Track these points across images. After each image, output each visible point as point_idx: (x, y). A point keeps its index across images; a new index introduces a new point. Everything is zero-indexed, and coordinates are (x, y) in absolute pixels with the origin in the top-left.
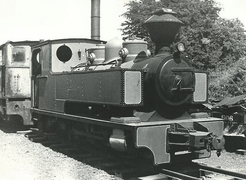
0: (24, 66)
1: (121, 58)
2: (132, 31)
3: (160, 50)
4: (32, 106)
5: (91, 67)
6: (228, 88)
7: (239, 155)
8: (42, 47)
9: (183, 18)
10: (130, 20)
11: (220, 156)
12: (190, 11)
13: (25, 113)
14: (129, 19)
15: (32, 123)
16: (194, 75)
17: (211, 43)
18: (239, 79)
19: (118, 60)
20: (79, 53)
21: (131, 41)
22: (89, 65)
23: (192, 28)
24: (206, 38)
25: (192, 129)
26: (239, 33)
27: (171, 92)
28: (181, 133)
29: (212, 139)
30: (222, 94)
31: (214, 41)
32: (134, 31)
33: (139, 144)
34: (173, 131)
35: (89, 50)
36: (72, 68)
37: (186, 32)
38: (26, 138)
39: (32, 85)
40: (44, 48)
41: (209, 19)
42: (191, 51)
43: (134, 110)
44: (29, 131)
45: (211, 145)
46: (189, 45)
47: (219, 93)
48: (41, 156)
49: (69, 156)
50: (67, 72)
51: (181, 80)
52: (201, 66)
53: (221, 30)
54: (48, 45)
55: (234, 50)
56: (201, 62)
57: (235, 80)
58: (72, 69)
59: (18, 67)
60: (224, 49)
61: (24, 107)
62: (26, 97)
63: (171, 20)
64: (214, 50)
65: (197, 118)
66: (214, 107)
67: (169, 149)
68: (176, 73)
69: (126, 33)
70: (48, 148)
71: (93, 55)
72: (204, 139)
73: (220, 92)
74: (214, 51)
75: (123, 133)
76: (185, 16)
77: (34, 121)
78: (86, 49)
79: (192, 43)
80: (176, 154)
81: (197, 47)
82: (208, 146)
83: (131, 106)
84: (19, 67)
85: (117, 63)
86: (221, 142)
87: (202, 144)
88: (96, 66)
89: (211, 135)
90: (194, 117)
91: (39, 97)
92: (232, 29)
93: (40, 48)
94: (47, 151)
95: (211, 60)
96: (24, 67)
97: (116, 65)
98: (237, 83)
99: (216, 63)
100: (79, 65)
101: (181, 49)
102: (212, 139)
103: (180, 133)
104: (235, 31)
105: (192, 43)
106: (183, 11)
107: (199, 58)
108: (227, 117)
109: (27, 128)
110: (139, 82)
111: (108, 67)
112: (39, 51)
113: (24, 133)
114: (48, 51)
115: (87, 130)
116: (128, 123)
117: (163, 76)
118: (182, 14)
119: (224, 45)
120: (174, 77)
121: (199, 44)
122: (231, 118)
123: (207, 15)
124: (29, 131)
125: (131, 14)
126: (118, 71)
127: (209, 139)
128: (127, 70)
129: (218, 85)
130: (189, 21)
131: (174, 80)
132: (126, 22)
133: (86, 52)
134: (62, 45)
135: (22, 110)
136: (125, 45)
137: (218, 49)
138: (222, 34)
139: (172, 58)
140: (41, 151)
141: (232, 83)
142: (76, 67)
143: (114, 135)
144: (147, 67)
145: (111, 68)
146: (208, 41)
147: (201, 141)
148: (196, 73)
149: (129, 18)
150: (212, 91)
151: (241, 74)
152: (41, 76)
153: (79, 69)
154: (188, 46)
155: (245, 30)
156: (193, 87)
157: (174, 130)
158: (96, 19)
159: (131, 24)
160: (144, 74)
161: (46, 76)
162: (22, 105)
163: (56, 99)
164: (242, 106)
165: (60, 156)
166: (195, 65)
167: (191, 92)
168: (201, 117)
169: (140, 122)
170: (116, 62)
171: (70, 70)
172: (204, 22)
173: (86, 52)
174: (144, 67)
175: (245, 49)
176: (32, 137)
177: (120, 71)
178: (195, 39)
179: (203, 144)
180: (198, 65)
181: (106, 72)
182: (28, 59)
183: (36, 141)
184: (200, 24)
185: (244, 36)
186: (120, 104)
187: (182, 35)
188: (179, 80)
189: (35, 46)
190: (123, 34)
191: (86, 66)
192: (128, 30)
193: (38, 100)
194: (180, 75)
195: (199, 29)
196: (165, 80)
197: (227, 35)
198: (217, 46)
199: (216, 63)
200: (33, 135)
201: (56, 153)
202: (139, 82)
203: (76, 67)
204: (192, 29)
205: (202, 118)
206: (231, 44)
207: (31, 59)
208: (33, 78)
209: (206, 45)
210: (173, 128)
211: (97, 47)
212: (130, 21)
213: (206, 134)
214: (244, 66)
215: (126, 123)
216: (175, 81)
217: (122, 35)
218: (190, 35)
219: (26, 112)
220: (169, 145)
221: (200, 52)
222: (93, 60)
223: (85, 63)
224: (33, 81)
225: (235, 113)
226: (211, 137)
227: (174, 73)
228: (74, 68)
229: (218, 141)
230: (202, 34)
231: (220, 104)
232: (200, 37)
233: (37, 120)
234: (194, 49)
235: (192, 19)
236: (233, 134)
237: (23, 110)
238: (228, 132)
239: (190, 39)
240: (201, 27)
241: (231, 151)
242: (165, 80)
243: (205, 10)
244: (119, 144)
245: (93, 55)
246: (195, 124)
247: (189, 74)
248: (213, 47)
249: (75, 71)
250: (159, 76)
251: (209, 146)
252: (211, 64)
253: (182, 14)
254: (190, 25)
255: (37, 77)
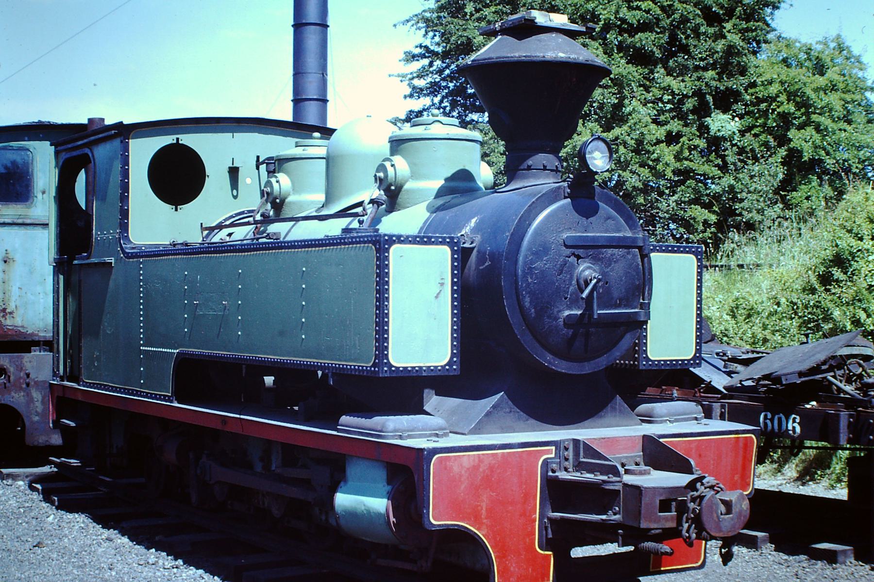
0: (28, 218)
1: (382, 192)
2: (444, 84)
3: (525, 166)
4: (55, 374)
5: (273, 228)
6: (798, 308)
7: (820, 564)
8: (132, 142)
9: (637, 36)
10: (437, 39)
11: (730, 564)
12: (663, 8)
13: (30, 400)
14: (433, 38)
15: (56, 439)
16: (646, 259)
17: (742, 133)
18: (837, 273)
19: (372, 201)
20: (234, 172)
21: (418, 131)
22: (267, 220)
23: (672, 75)
24: (724, 112)
25: (637, 464)
26: (848, 97)
27: (562, 323)
28: (591, 476)
29: (701, 498)
30: (773, 332)
31: (754, 126)
32: (451, 85)
33: (435, 520)
34: (566, 469)
35: (269, 161)
36: (206, 229)
37: (647, 89)
38: (35, 496)
39: (56, 291)
40: (102, 153)
41: (734, 38)
42: (667, 164)
43: (426, 391)
44: (46, 469)
45: (698, 521)
46: (659, 142)
47: (765, 328)
48: (87, 562)
49: (188, 562)
50: (186, 245)
51: (599, 280)
52: (706, 223)
53: (782, 83)
54: (117, 143)
55: (829, 162)
56: (705, 206)
57: (826, 280)
58: (206, 232)
59: (7, 221)
60: (793, 160)
61: (28, 375)
62: (37, 339)
63: (561, 55)
64: (756, 159)
65: (661, 422)
66: (734, 381)
67: (550, 536)
68: (580, 252)
69: (417, 92)
70: (113, 533)
71: (283, 182)
72: (675, 500)
73: (770, 323)
74: (753, 164)
75: (380, 474)
76: (644, 27)
77: (65, 431)
78: (258, 157)
79: (669, 134)
80: (578, 552)
81: (690, 149)
82: (686, 526)
83: (411, 374)
84: (9, 221)
85: (369, 211)
86: (735, 509)
87: (666, 519)
88: (293, 223)
89: (698, 484)
90: (648, 418)
91: (80, 340)
92: (821, 81)
93: (87, 151)
94: (108, 544)
95: (742, 200)
96: (28, 221)
97: (361, 222)
98: (829, 290)
99: (760, 211)
100: (232, 217)
101: (596, 162)
102: (701, 498)
103: (588, 475)
104: (834, 88)
105: (669, 134)
106: (638, 8)
107: (696, 191)
108: (780, 419)
109: (38, 456)
110: (442, 284)
111: (334, 228)
112: (84, 162)
113: (27, 477)
114: (118, 166)
115: (259, 467)
116: (401, 437)
117: (532, 262)
118: (635, 22)
119: (790, 140)
120: (573, 267)
121: (700, 137)
122: (794, 425)
123: (728, 26)
124: (46, 469)
125: (439, 18)
126: (365, 242)
127: (693, 500)
128: (400, 239)
129: (765, 299)
130: (660, 47)
131: (571, 278)
132: (421, 46)
133: (258, 168)
134: (167, 140)
135: (21, 389)
136: (397, 144)
137: (770, 156)
138: (783, 98)
139: (565, 198)
140: (89, 542)
141: (813, 291)
142: (220, 227)
143: (350, 483)
144: (475, 230)
145: (346, 230)
146: (732, 123)
147: (665, 506)
148: (658, 251)
149: (431, 34)
150: (741, 318)
151: (846, 255)
152: (88, 257)
153: (230, 235)
154: (655, 144)
155: (869, 83)
156: (642, 306)
157: (569, 464)
158: (311, 36)
159: (445, 55)
160: (461, 256)
161: (107, 260)
162: (20, 368)
163: (142, 345)
164: (833, 377)
165: (157, 562)
166: (683, 219)
167: (638, 325)
168: (676, 418)
169: (446, 435)
170: (364, 209)
171: (196, 238)
172: (717, 52)
173: (258, 168)
174: (464, 226)
175: (869, 159)
176: (56, 492)
177: (374, 243)
178: (681, 116)
179: (672, 516)
180: (694, 219)
181: (326, 245)
182: (44, 193)
183: (67, 506)
184: (701, 59)
185: (868, 108)
186: (371, 367)
187: (634, 103)
188: (591, 280)
189: (70, 146)
190: (411, 96)
191: (256, 222)
192: (429, 80)
193: (80, 352)
194: (596, 259)
195: (699, 79)
196: (537, 278)
197: (804, 104)
198: (766, 144)
199: (760, 211)
200: (60, 485)
201: (140, 549)
202: (442, 284)
203: (220, 227)
204: (669, 79)
205: (677, 421)
206: (817, 137)
207: (53, 194)
208: (62, 266)
209: (724, 139)
210: (567, 459)
211: (299, 152)
212: (438, 44)
213: (681, 479)
214: (859, 226)
215: (393, 437)
216: (574, 282)
217: (405, 97)
218: (663, 103)
219: (37, 395)
220: (549, 519)
221: (700, 166)
222: (283, 201)
223: (252, 211)
224: (61, 277)
225: (808, 406)
226: (697, 490)
227: (573, 254)
228: (211, 229)
229: (723, 508)
230: (709, 98)
231: (757, 370)
232: (702, 111)
233: (73, 424)
234: (678, 157)
235: (673, 38)
236: (814, 486)
237: (24, 386)
238: (797, 479)
239: (662, 118)
240: (708, 70)
241: (791, 551)
242: (537, 278)
243: (722, 7)
244: (369, 516)
245: (283, 182)
246: (648, 441)
247: (630, 257)
248: (752, 150)
249: (216, 239)
250: (516, 262)
251: (689, 527)
252: (740, 215)
253: (635, 22)
254: (664, 63)
255: (76, 262)
